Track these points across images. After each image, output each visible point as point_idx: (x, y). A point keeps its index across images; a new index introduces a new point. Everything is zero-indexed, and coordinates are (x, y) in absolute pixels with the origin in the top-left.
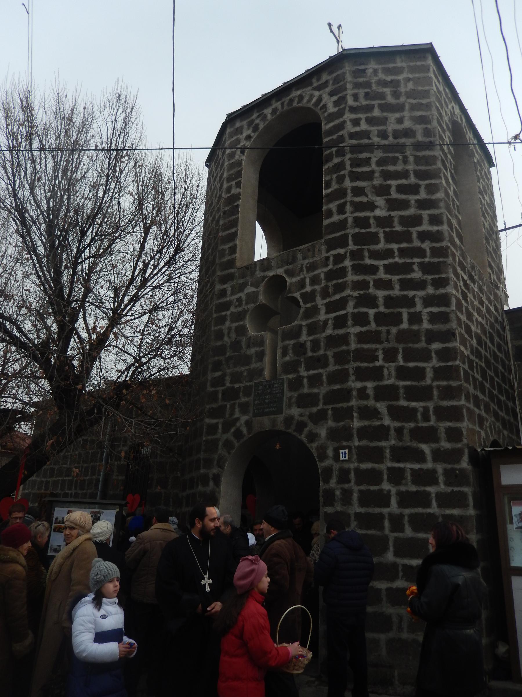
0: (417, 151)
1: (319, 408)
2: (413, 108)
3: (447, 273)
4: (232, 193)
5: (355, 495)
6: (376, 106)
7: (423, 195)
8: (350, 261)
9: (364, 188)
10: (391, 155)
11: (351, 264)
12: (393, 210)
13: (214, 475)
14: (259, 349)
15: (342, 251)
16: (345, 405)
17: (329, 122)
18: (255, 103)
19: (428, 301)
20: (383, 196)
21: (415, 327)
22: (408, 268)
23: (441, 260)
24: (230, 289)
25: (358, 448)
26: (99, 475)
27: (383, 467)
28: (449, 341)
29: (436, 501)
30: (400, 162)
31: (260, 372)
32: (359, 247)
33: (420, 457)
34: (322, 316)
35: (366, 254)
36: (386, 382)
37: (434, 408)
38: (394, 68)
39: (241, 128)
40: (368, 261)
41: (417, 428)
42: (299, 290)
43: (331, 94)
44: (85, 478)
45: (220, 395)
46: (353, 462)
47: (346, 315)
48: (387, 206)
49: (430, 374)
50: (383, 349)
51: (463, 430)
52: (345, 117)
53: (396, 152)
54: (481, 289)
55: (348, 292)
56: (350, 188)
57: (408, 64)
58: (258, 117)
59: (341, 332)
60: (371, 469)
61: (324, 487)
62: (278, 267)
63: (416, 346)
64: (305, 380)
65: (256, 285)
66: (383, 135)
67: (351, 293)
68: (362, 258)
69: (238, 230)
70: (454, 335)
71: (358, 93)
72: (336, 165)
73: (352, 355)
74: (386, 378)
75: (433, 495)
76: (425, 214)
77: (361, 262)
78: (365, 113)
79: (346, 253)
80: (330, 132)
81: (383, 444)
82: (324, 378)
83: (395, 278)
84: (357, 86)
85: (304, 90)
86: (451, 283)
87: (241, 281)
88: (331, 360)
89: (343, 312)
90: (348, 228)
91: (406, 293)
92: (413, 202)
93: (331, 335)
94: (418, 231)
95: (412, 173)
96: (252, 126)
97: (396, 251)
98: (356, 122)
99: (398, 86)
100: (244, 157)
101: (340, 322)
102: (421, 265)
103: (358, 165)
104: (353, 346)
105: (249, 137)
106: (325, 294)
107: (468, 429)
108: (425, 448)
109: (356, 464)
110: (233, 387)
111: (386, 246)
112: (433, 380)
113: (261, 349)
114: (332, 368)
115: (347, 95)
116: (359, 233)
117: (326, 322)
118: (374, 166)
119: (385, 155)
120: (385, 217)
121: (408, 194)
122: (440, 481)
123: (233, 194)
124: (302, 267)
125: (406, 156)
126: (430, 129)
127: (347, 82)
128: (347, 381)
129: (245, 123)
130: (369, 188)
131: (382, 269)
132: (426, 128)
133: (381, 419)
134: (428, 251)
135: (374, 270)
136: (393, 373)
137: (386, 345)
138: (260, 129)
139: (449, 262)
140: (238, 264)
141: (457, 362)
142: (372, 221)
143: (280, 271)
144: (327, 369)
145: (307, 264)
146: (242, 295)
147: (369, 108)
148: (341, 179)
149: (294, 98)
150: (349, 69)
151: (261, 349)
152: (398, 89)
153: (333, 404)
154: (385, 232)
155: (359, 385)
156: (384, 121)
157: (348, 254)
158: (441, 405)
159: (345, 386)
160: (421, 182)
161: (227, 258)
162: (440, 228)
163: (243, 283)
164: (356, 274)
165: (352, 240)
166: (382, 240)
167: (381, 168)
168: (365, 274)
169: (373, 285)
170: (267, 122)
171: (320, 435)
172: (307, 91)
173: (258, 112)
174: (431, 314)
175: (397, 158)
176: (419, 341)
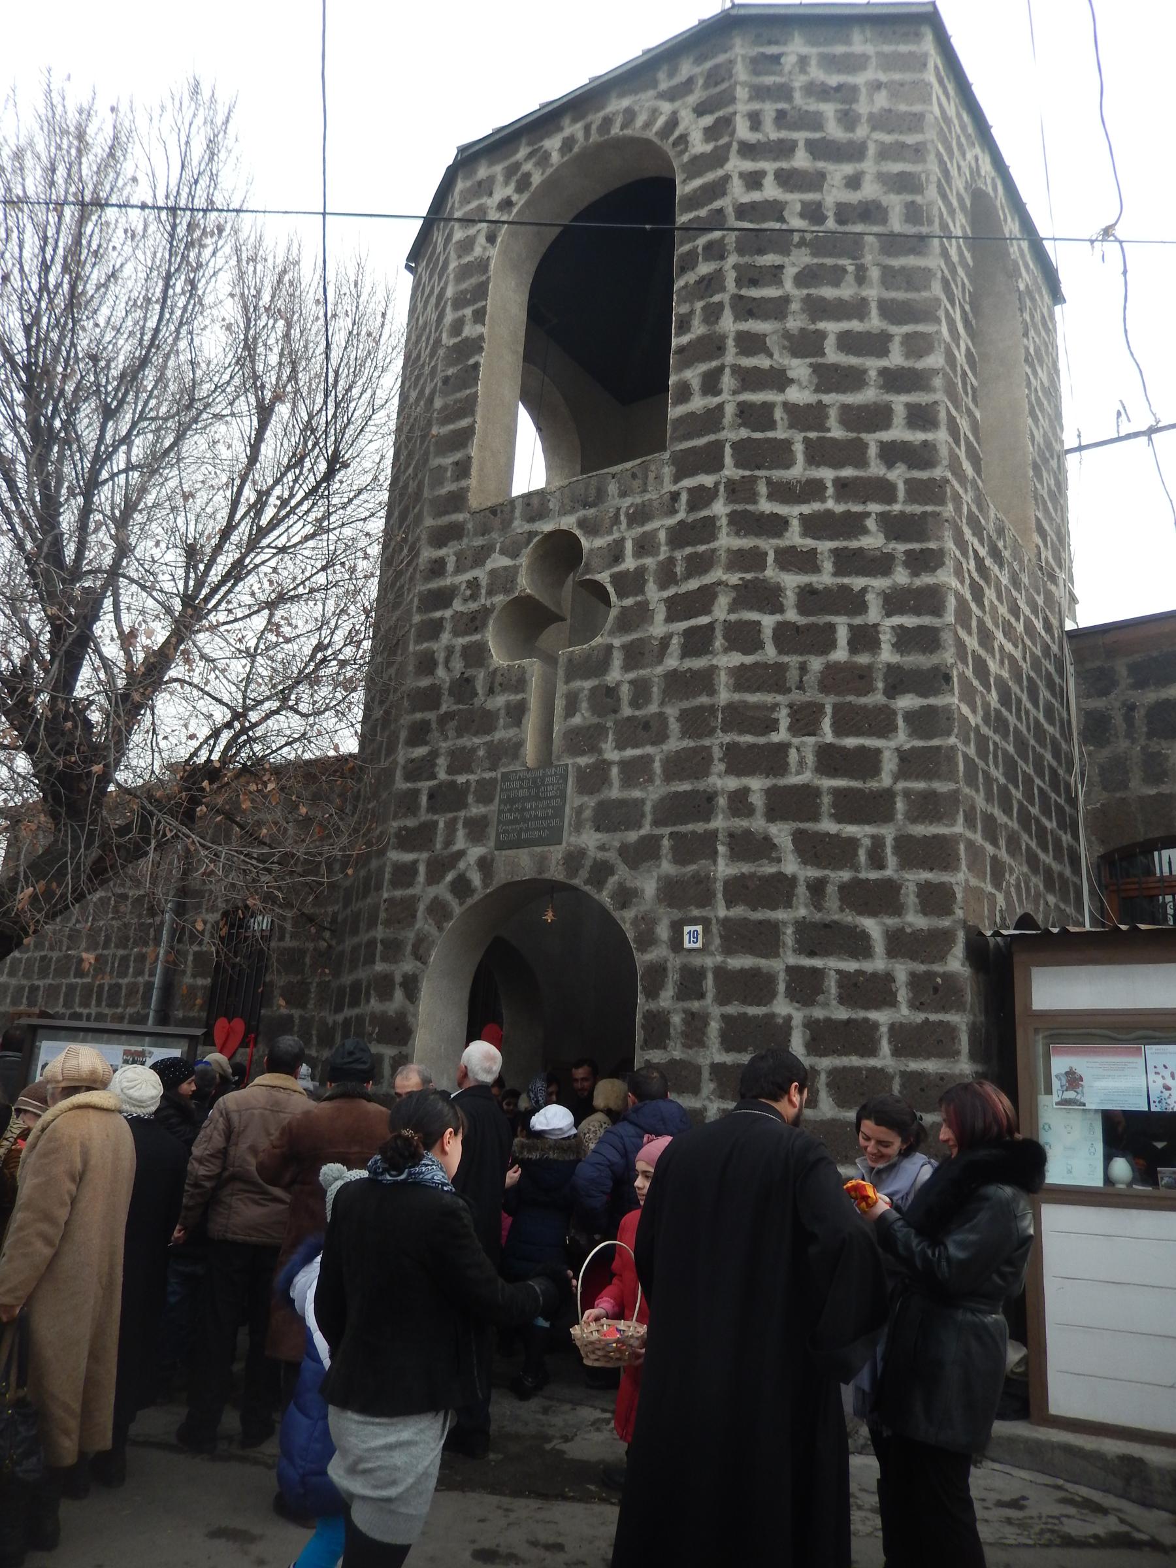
1: (643, 832)
2: (885, 153)
3: (940, 538)
4: (464, 335)
5: (714, 1027)
6: (801, 144)
7: (896, 358)
8: (725, 505)
9: (765, 336)
10: (829, 261)
11: (728, 510)
12: (828, 391)
13: (405, 976)
14: (514, 698)
15: (708, 480)
16: (700, 827)
17: (690, 177)
19: (895, 602)
21: (863, 659)
22: (853, 525)
23: (929, 508)
25: (725, 922)
27: (776, 966)
28: (936, 692)
29: (890, 1042)
30: (850, 278)
31: (514, 749)
32: (747, 473)
33: (859, 945)
34: (658, 628)
35: (763, 489)
36: (794, 780)
37: (895, 839)
39: (491, 180)
40: (766, 506)
41: (857, 883)
42: (610, 566)
44: (120, 981)
45: (424, 799)
46: (712, 954)
47: (711, 626)
48: (815, 381)
49: (889, 764)
50: (791, 706)
53: (840, 255)
54: (1015, 581)
55: (717, 574)
56: (732, 336)
57: (879, 49)
58: (530, 156)
61: (647, 1007)
62: (564, 512)
63: (863, 700)
64: (615, 771)
65: (512, 552)
67: (724, 578)
68: (753, 498)
70: (947, 678)
72: (702, 279)
74: (793, 770)
75: (884, 1029)
76: (899, 402)
77: (750, 507)
79: (717, 484)
80: (694, 201)
81: (780, 915)
82: (657, 766)
83: (825, 546)
84: (760, 93)
85: (638, 97)
86: (947, 562)
87: (479, 542)
88: (674, 726)
89: (704, 620)
91: (846, 580)
92: (873, 374)
93: (675, 670)
94: (881, 442)
96: (515, 178)
97: (829, 484)
98: (754, 181)
100: (494, 252)
101: (697, 642)
102: (883, 518)
103: (754, 283)
104: (724, 696)
105: (507, 204)
106: (667, 576)
108: (872, 926)
109: (719, 959)
110: (453, 783)
111: (808, 472)
112: (896, 778)
113: (519, 697)
114: (675, 743)
117: (665, 642)
118: (789, 286)
119: (815, 261)
122: (899, 999)
123: (467, 338)
124: (617, 515)
126: (921, 206)
127: (736, 83)
128: (707, 774)
129: (498, 169)
130: (775, 337)
131: (795, 524)
132: (913, 202)
133: (779, 860)
134: (901, 487)
135: (778, 525)
136: (810, 759)
137: (797, 697)
139: (946, 515)
142: (778, 414)
143: (568, 522)
145: (628, 508)
146: (481, 574)
147: (784, 149)
148: (713, 314)
151: (519, 697)
155: (732, 783)
156: (816, 181)
157: (722, 488)
159: (701, 785)
160: (893, 329)
161: (450, 487)
162: (929, 436)
163: (482, 547)
164: (737, 534)
166: (800, 457)
167: (805, 292)
168: (758, 535)
170: (549, 171)
171: (643, 891)
174: (900, 631)
176: (869, 690)
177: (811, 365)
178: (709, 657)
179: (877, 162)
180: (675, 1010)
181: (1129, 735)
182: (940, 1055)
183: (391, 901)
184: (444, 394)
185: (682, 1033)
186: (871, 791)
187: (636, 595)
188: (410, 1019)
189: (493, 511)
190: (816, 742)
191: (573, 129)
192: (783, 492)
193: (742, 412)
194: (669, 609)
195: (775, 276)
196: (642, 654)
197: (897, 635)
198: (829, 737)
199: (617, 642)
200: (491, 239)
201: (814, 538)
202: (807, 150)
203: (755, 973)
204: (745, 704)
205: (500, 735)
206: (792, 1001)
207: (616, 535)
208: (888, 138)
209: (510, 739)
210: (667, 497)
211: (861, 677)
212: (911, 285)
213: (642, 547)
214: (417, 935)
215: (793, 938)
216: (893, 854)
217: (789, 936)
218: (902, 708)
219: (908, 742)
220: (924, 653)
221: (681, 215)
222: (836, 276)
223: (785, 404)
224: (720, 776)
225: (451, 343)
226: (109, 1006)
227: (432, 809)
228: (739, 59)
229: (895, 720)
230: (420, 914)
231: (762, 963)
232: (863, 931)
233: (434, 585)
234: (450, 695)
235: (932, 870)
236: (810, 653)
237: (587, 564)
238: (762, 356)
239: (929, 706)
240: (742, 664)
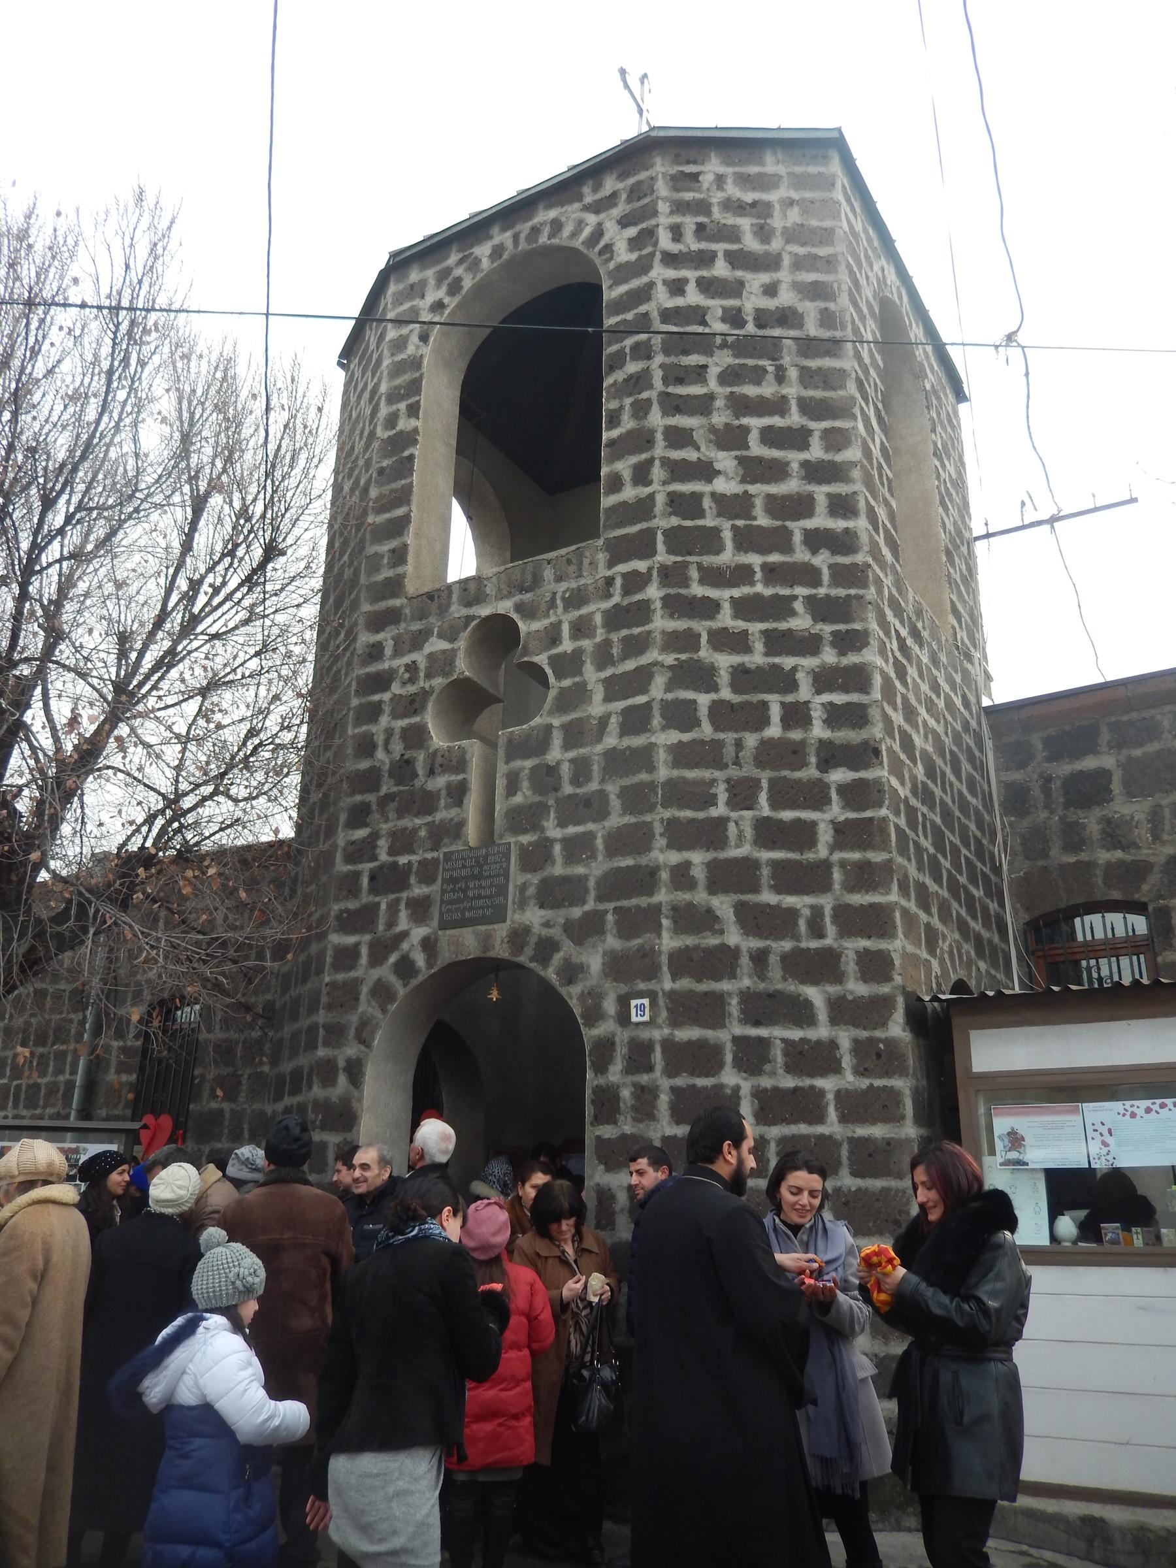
2: (799, 264)
3: (864, 620)
4: (398, 428)
5: (664, 1099)
6: (720, 255)
7: (816, 452)
8: (658, 589)
9: (692, 430)
10: (750, 362)
11: (662, 593)
14: (457, 778)
15: (641, 565)
16: (643, 901)
17: (616, 283)
19: (824, 680)
21: (796, 735)
23: (853, 592)
25: (671, 995)
26: (74, 1072)
28: (866, 766)
29: (837, 1109)
30: (770, 378)
31: (456, 829)
32: (679, 559)
33: (802, 1013)
35: (694, 574)
36: (733, 853)
37: (834, 909)
38: (761, 175)
39: (423, 283)
40: (698, 590)
41: (798, 953)
42: (548, 648)
43: (624, 222)
46: (659, 1027)
47: (648, 705)
48: (741, 472)
49: (825, 836)
50: (728, 781)
51: (894, 955)
53: (760, 357)
54: (935, 660)
56: (660, 430)
57: (790, 170)
58: (461, 262)
59: (638, 741)
61: (596, 1083)
62: (500, 597)
63: (797, 775)
64: (557, 848)
65: (450, 635)
67: (660, 658)
68: (685, 582)
69: (411, 511)
70: (877, 752)
72: (631, 377)
73: (660, 792)
74: (733, 843)
75: (830, 1097)
76: (821, 492)
77: (683, 591)
78: (696, 269)
79: (650, 569)
80: (621, 305)
81: (725, 986)
82: (599, 842)
83: (755, 628)
84: (680, 207)
85: (564, 209)
86: (872, 642)
87: (416, 626)
88: (615, 803)
89: (641, 699)
91: (777, 660)
92: (795, 466)
94: (805, 530)
95: (793, 403)
96: (446, 282)
97: (757, 569)
98: (677, 287)
99: (770, 216)
100: (427, 351)
101: (635, 721)
102: (810, 601)
103: (680, 381)
104: (664, 772)
105: (439, 306)
106: (604, 658)
108: (815, 995)
109: (666, 1031)
110: (395, 864)
111: (736, 558)
112: (833, 849)
113: (460, 777)
114: (616, 820)
115: (658, 226)
117: (604, 721)
118: (713, 384)
119: (737, 361)
120: (736, 496)
123: (401, 432)
125: (782, 366)
128: (648, 849)
129: (430, 274)
130: (701, 432)
131: (726, 608)
132: (826, 309)
135: (709, 608)
136: (749, 832)
137: (733, 772)
138: (465, 289)
141: (884, 812)
142: (707, 503)
143: (505, 607)
145: (564, 592)
146: (419, 657)
147: (706, 259)
148: (642, 409)
149: (541, 224)
150: (662, 169)
151: (460, 777)
152: (768, 221)
154: (734, 527)
155: (674, 857)
156: (735, 289)
157: (655, 573)
159: (643, 860)
160: (812, 425)
161: (386, 573)
162: (850, 524)
163: (420, 631)
164: (671, 616)
167: (729, 390)
170: (480, 276)
171: (589, 966)
172: (570, 213)
174: (830, 708)
176: (803, 764)
177: (736, 457)
178: (648, 735)
179: (792, 272)
180: (624, 1084)
181: (1047, 806)
182: (886, 1120)
183: (333, 985)
184: (380, 484)
185: (633, 1107)
188: (354, 1104)
190: (754, 816)
191: (501, 237)
192: (713, 577)
193: (672, 501)
194: (606, 689)
195: (699, 375)
197: (828, 711)
198: (765, 810)
199: (556, 722)
200: (424, 338)
201: (745, 620)
203: (702, 1044)
206: (739, 1071)
207: (553, 619)
208: (801, 250)
209: (452, 819)
211: (795, 753)
213: (579, 630)
214: (361, 1018)
216: (832, 923)
218: (835, 782)
222: (757, 375)
223: (713, 494)
224: (661, 851)
226: (27, 1107)
227: (373, 890)
228: (660, 176)
231: (709, 1034)
233: (372, 669)
235: (869, 937)
236: (745, 729)
237: (524, 647)
238: (690, 449)
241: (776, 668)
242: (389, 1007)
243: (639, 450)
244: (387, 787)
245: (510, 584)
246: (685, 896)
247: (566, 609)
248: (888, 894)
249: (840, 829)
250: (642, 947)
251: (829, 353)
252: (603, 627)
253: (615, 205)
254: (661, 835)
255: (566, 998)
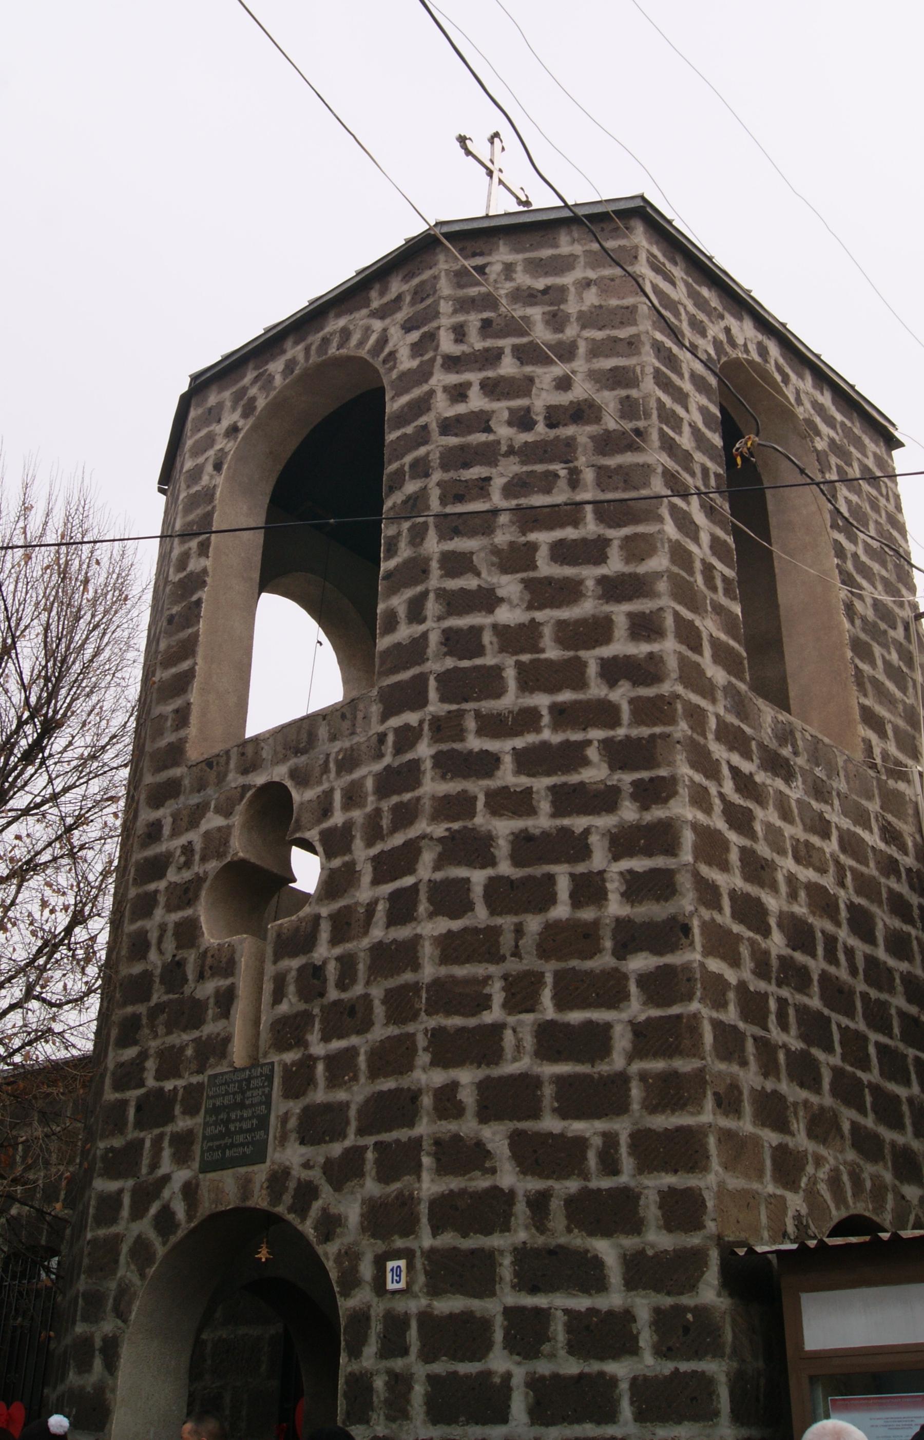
0: (604, 455)
2: (596, 351)
3: (671, 764)
4: (189, 569)
5: (419, 1390)
6: (508, 351)
7: (615, 564)
8: (429, 745)
9: (472, 553)
10: (539, 468)
11: (432, 751)
12: (541, 608)
13: (105, 1339)
14: (224, 983)
15: (411, 718)
16: (402, 1134)
17: (398, 394)
18: (251, 347)
20: (517, 572)
21: (587, 914)
23: (657, 730)
24: (169, 820)
25: (430, 1255)
28: (673, 948)
29: (632, 1403)
30: (562, 483)
31: (220, 1046)
32: (454, 707)
34: (364, 893)
35: (471, 724)
36: (510, 1068)
37: (632, 1136)
38: (554, 258)
39: (220, 405)
40: (474, 743)
41: (586, 1194)
42: (319, 821)
43: (408, 327)
45: (131, 1112)
46: (416, 1296)
47: (415, 887)
48: (527, 597)
49: (622, 1040)
50: (505, 977)
51: (707, 1195)
52: (433, 381)
53: (551, 461)
54: (820, 791)
55: (422, 826)
56: (436, 557)
57: (587, 248)
58: (256, 379)
59: (402, 933)
60: (463, 1313)
61: (349, 1369)
62: (277, 762)
63: (589, 964)
64: (320, 1068)
65: (226, 811)
66: (523, 420)
67: (429, 830)
68: (460, 735)
69: (196, 664)
70: (686, 930)
71: (465, 321)
72: (409, 498)
73: (424, 995)
74: (509, 1057)
75: (624, 1386)
76: (620, 612)
77: (457, 746)
78: (480, 370)
79: (421, 722)
80: (402, 419)
81: (496, 1241)
82: (362, 1059)
83: (541, 783)
84: (464, 305)
85: (352, 317)
86: (681, 791)
87: (195, 799)
88: (379, 1010)
89: (408, 881)
90: (428, 659)
91: (566, 822)
92: (590, 583)
93: (380, 942)
94: (602, 659)
96: (242, 403)
97: (545, 712)
98: (458, 393)
99: (564, 300)
100: (220, 480)
102: (606, 744)
103: (460, 498)
104: (429, 971)
105: (233, 430)
106: (374, 834)
107: (722, 1191)
109: (424, 1302)
110: (161, 1089)
111: (520, 700)
113: (228, 982)
114: (380, 1032)
115: (439, 328)
116: (456, 669)
117: (371, 908)
118: (497, 499)
119: (525, 468)
120: (521, 626)
121: (581, 564)
122: (642, 1344)
123: (192, 573)
124: (327, 762)
125: (576, 468)
126: (636, 400)
127: (440, 298)
128: (410, 1068)
129: (227, 395)
130: (482, 555)
131: (508, 762)
132: (628, 397)
133: (493, 1171)
134: (625, 708)
136: (529, 1042)
137: (512, 966)
138: (259, 409)
139: (678, 735)
140: (194, 753)
141: (695, 1006)
142: (487, 638)
143: (280, 773)
144: (369, 1036)
145: (338, 753)
146: (194, 837)
147: (492, 357)
148: (418, 536)
149: (331, 334)
150: (446, 267)
151: (228, 982)
152: (562, 307)
153: (379, 1132)
154: (519, 665)
155: (438, 1078)
156: (525, 386)
157: (426, 727)
158: (648, 1125)
159: (405, 1082)
160: (611, 533)
161: (170, 738)
162: (655, 647)
163: (198, 805)
164: (443, 777)
165: (437, 689)
168: (466, 777)
169: (487, 805)
170: (273, 394)
171: (346, 1218)
172: (358, 320)
173: (256, 368)
175: (556, 476)
176: (594, 951)
177: (523, 581)
178: (414, 924)
180: (378, 1372)
183: (94, 1242)
184: (169, 634)
185: (386, 1401)
186: (601, 1076)
187: (344, 854)
188: (109, 1395)
189: (209, 763)
190: (536, 1020)
191: (294, 351)
193: (447, 639)
194: (375, 869)
195: (482, 488)
196: (348, 924)
197: (627, 881)
198: (548, 1010)
200: (218, 467)
201: (529, 775)
202: (513, 356)
203: (466, 1318)
204: (453, 979)
205: (210, 1028)
206: (511, 1353)
207: (325, 786)
208: (599, 335)
209: (218, 1034)
210: (374, 739)
211: (586, 936)
212: (628, 484)
213: (350, 798)
214: (119, 1285)
215: (511, 1270)
216: (629, 1154)
217: (506, 1268)
218: (634, 971)
219: (643, 1011)
220: (658, 900)
221: (390, 433)
222: (548, 482)
223: (495, 626)
224: (424, 1070)
225: (177, 579)
227: (140, 1125)
228: (443, 274)
229: (626, 986)
230: (122, 1259)
231: (475, 1305)
232: (596, 1257)
233: (150, 852)
234: (161, 982)
235: (676, 1172)
236: (526, 911)
237: (297, 821)
238: (469, 576)
239: (666, 966)
240: (449, 931)
241: (565, 832)
242: (147, 1270)
243: (415, 582)
244: (158, 996)
245: (286, 747)
246: (451, 1126)
247: (338, 773)
248: (699, 1113)
249: (639, 1030)
250: (400, 1194)
251: (632, 447)
252: (374, 793)
253: (400, 308)
254: (425, 1049)
255: (323, 1259)
